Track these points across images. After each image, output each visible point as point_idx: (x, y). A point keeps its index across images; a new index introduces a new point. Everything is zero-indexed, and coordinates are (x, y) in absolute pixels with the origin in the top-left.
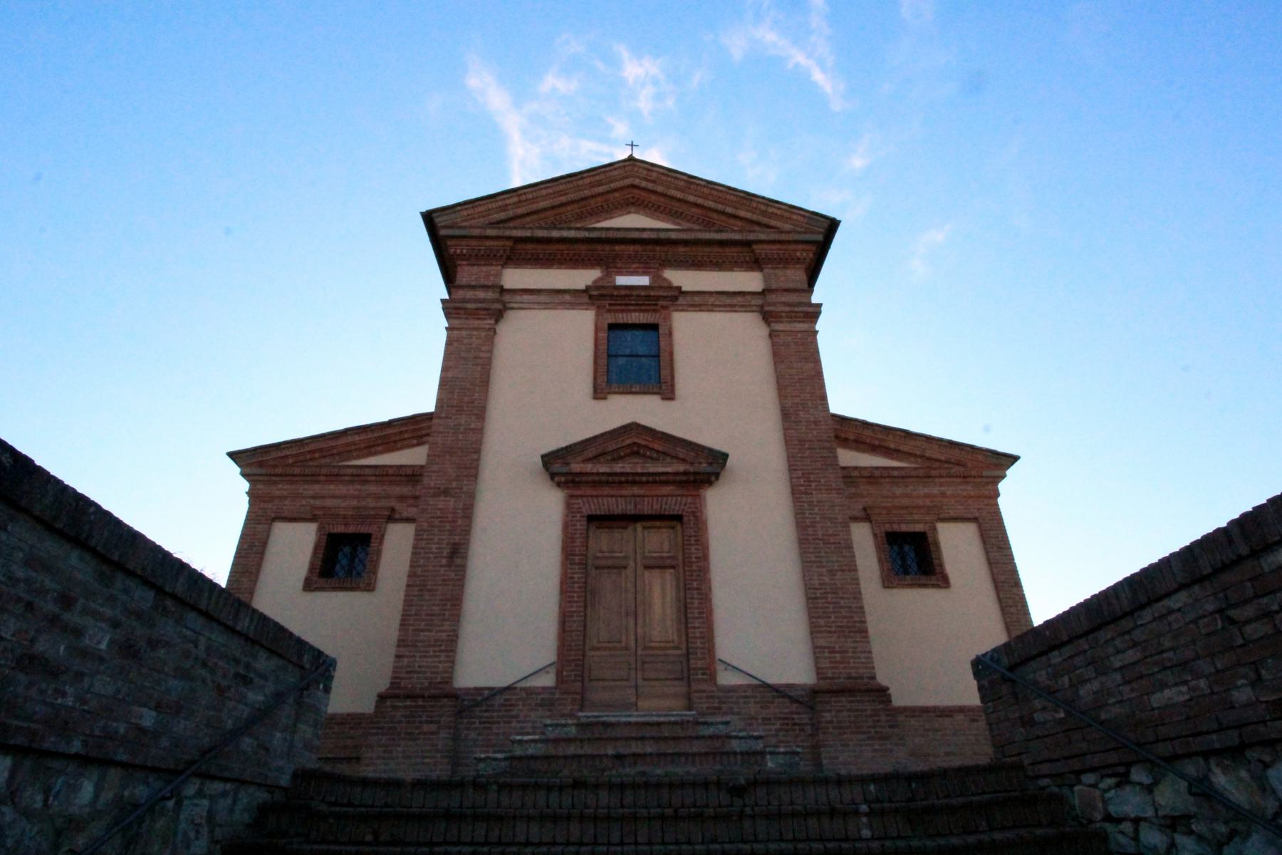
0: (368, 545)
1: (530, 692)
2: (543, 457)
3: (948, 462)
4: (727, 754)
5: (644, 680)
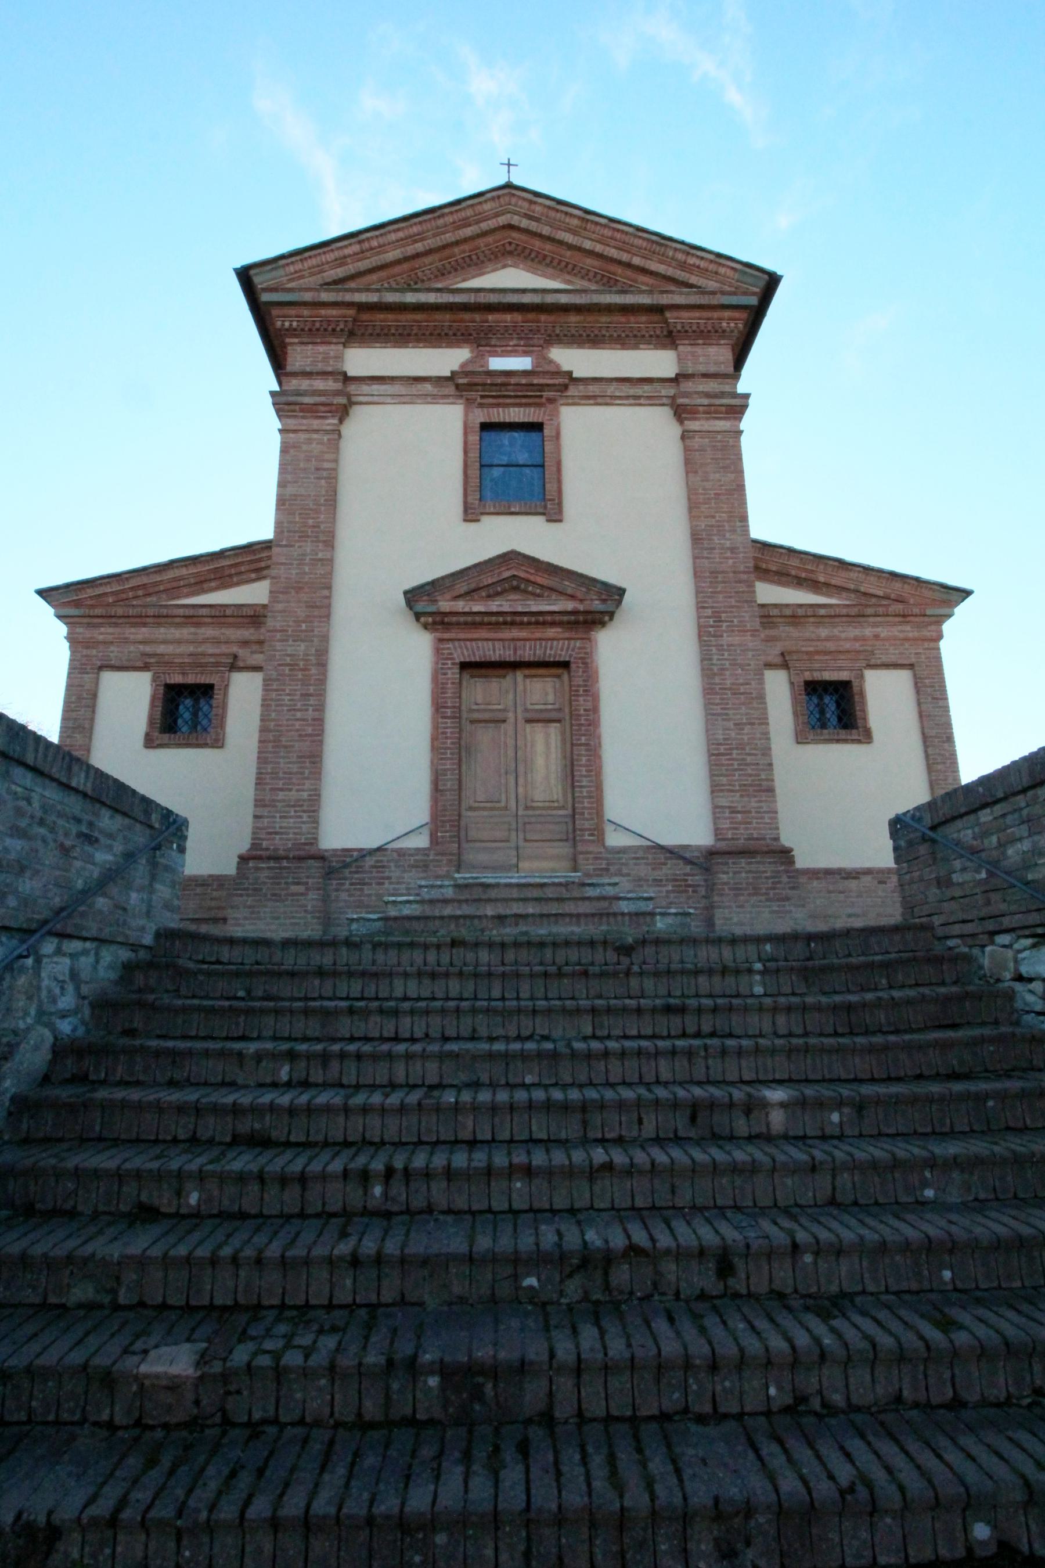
0: (211, 697)
1: (401, 853)
2: (406, 593)
3: (886, 597)
4: (615, 914)
5: (526, 840)
